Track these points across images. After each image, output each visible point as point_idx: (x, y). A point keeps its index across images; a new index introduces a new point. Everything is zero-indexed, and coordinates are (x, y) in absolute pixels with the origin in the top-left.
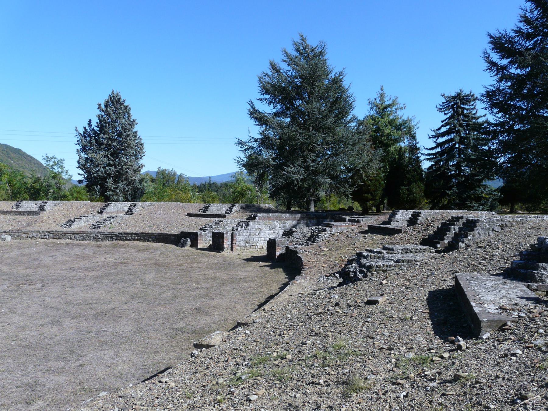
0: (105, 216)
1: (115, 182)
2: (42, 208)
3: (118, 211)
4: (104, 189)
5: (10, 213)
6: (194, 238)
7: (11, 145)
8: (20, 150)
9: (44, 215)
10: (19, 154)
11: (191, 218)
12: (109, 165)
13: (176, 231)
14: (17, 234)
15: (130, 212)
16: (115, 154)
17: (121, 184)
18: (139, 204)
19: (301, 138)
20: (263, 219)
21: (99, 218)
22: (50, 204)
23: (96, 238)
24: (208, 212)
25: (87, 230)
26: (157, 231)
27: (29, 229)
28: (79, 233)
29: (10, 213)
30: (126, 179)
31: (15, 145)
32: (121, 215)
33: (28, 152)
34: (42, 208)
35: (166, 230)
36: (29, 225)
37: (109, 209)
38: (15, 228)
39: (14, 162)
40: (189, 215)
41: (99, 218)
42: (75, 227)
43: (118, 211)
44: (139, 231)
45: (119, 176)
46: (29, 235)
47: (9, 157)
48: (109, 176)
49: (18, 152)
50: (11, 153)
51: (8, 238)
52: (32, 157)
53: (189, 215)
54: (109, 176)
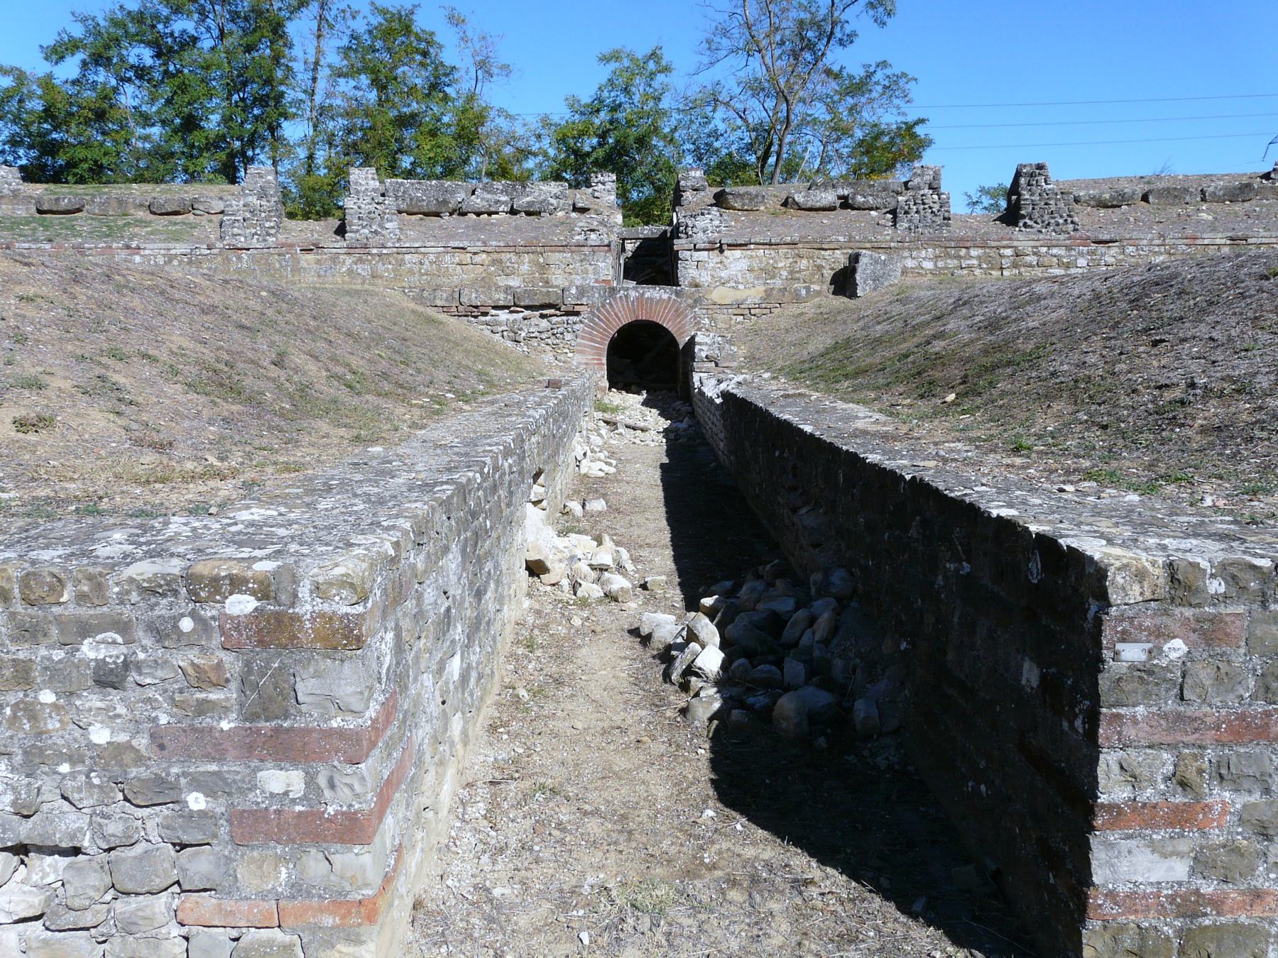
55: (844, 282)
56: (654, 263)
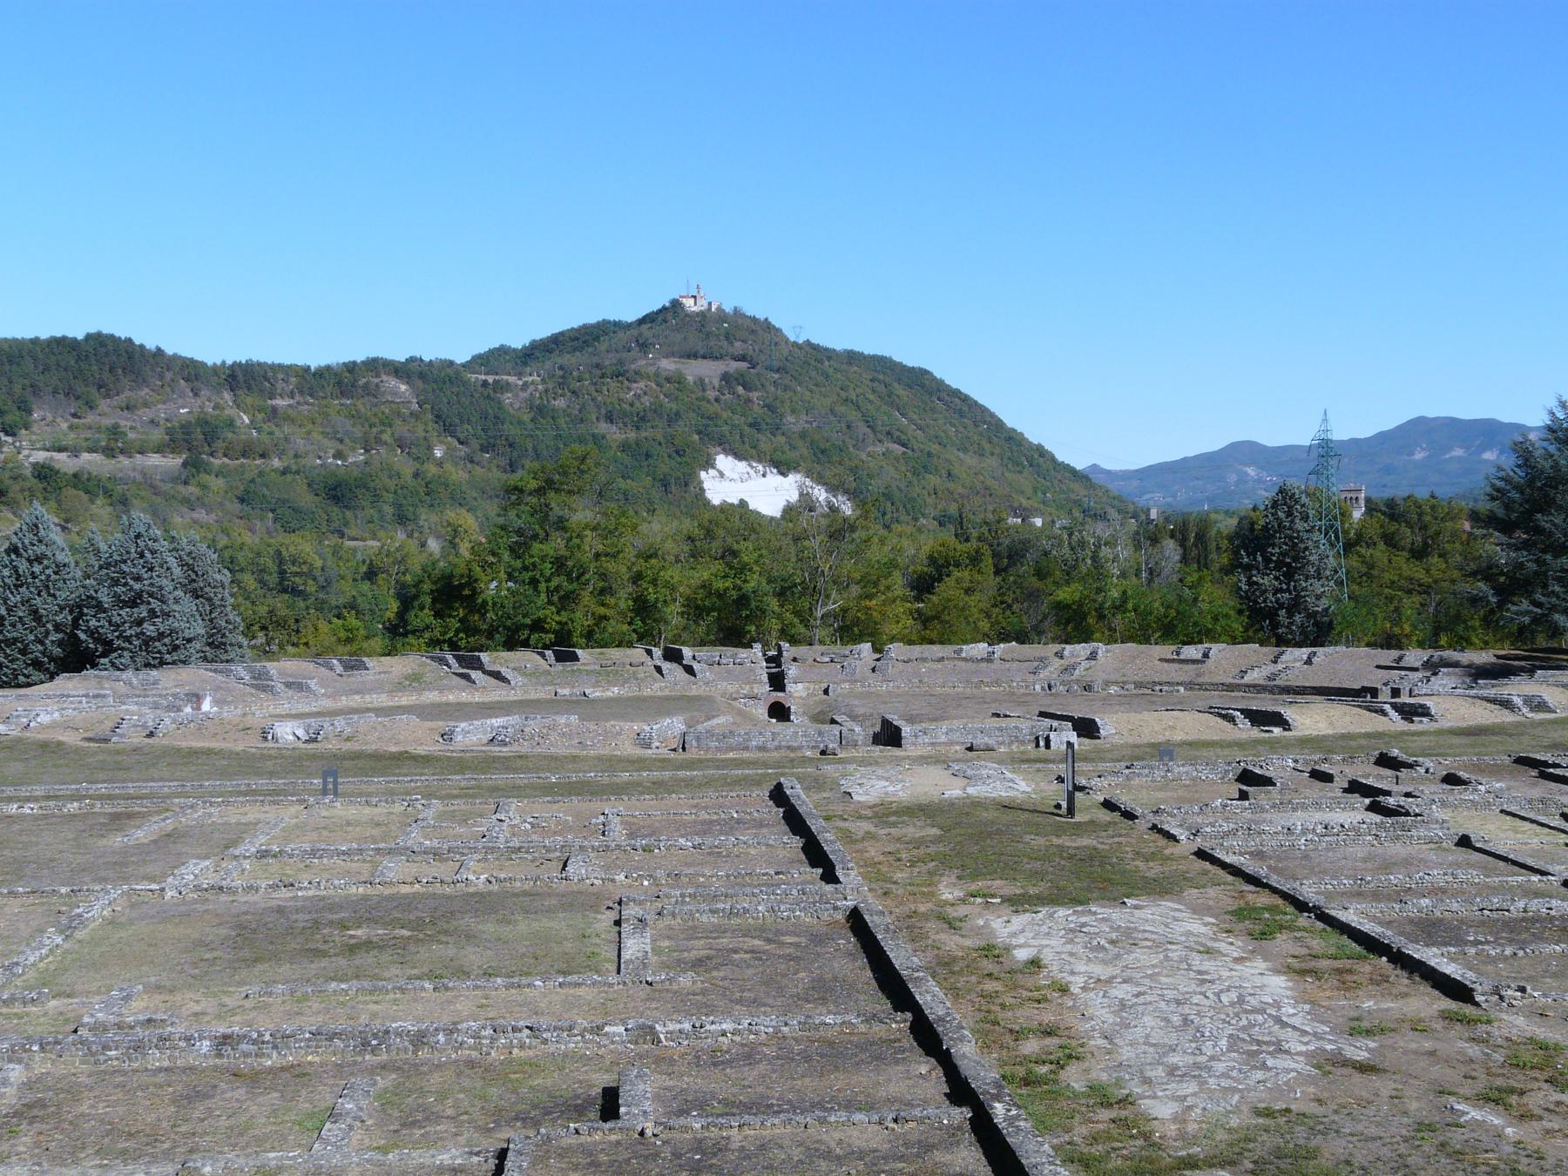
0: (1280, 666)
1: (1290, 615)
2: (1206, 655)
3: (1295, 660)
4: (1275, 625)
5: (1173, 661)
6: (1374, 692)
7: (897, 358)
8: (925, 372)
9: (1210, 663)
10: (923, 386)
11: (848, 942)
12: (1281, 591)
13: (1357, 687)
14: (1190, 686)
15: (1309, 662)
16: (1289, 576)
17: (1298, 618)
18: (1320, 650)
19: (1532, 566)
20: (1448, 674)
21: (1272, 668)
22: (1216, 649)
23: (1272, 692)
24: (1402, 664)
25: (1262, 682)
26: (1338, 685)
27: (1201, 680)
28: (1254, 686)
29: (1173, 661)
30: (1306, 609)
31: (909, 356)
32: (1298, 664)
33: (953, 381)
34: (1206, 655)
35: (1347, 685)
36: (1198, 675)
37: (1284, 658)
38: (1187, 679)
39: (911, 421)
40: (1378, 667)
41: (1272, 668)
42: (1248, 679)
43: (1295, 660)
44: (1318, 684)
45: (1295, 606)
46: (1202, 687)
47: (892, 404)
48: (1281, 606)
49: (920, 381)
50: (900, 390)
51: (1182, 689)
52: (965, 399)
53: (1378, 667)
54: (1281, 606)
55: (826, 692)
56: (777, 682)
